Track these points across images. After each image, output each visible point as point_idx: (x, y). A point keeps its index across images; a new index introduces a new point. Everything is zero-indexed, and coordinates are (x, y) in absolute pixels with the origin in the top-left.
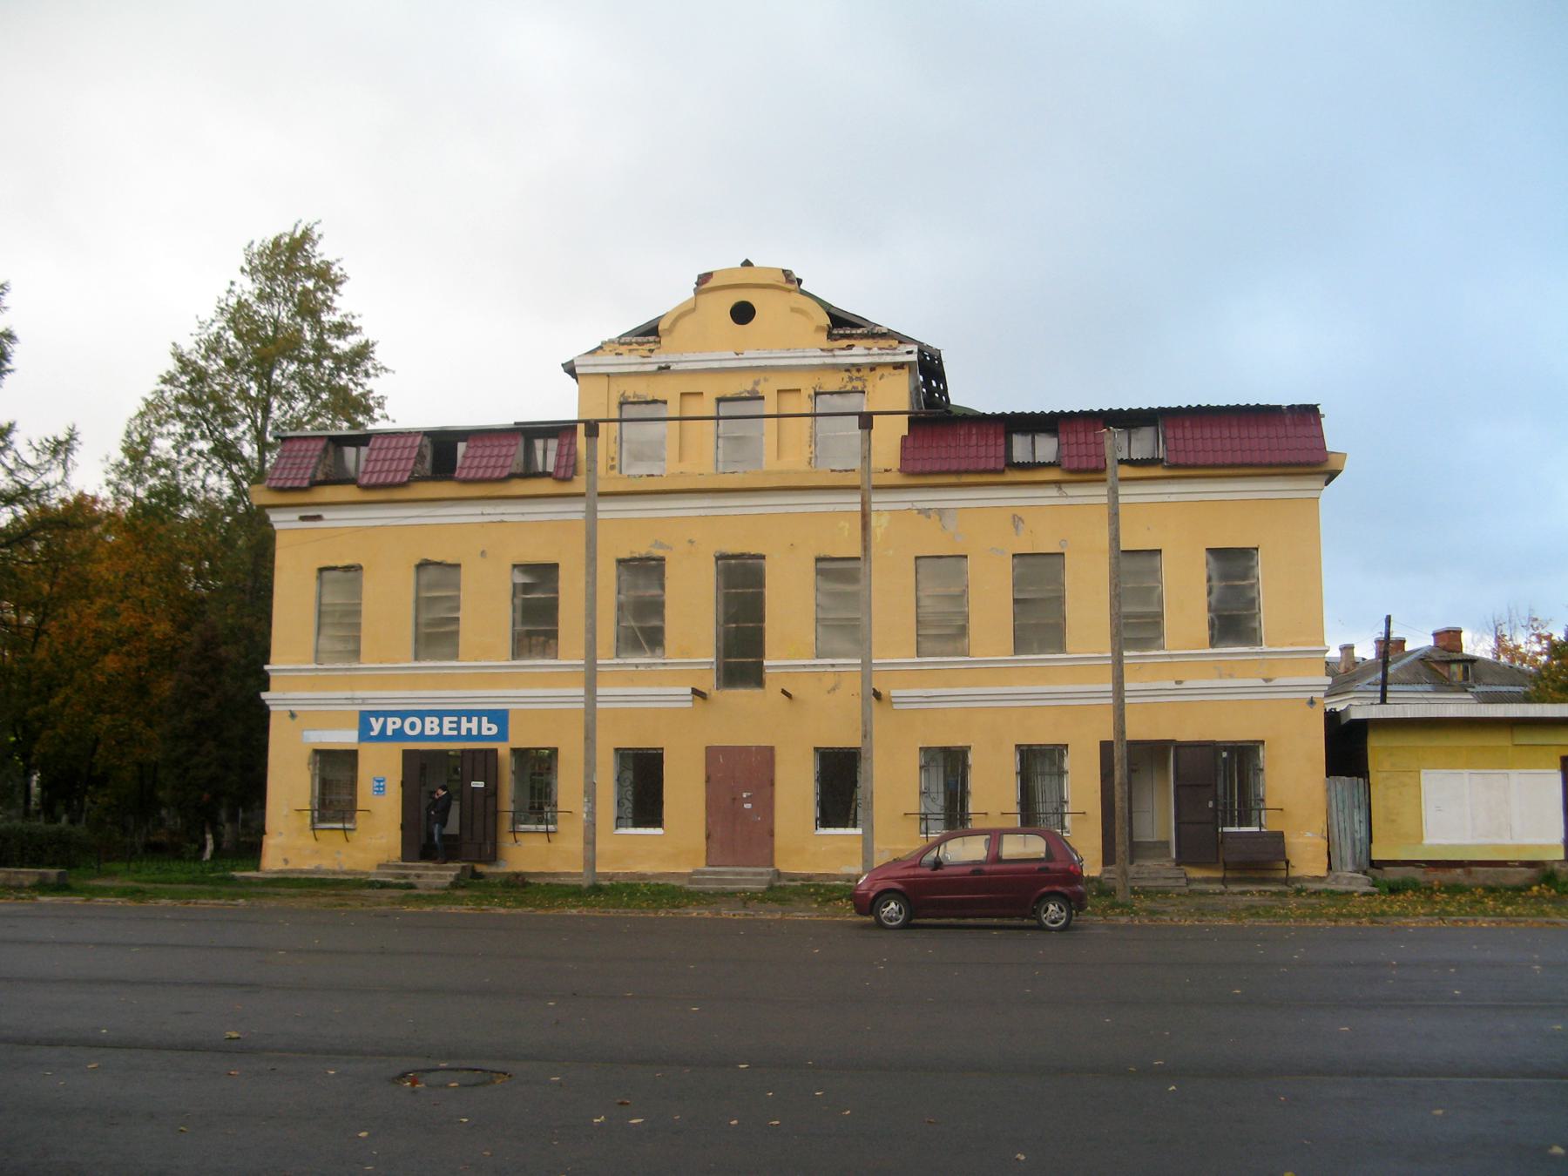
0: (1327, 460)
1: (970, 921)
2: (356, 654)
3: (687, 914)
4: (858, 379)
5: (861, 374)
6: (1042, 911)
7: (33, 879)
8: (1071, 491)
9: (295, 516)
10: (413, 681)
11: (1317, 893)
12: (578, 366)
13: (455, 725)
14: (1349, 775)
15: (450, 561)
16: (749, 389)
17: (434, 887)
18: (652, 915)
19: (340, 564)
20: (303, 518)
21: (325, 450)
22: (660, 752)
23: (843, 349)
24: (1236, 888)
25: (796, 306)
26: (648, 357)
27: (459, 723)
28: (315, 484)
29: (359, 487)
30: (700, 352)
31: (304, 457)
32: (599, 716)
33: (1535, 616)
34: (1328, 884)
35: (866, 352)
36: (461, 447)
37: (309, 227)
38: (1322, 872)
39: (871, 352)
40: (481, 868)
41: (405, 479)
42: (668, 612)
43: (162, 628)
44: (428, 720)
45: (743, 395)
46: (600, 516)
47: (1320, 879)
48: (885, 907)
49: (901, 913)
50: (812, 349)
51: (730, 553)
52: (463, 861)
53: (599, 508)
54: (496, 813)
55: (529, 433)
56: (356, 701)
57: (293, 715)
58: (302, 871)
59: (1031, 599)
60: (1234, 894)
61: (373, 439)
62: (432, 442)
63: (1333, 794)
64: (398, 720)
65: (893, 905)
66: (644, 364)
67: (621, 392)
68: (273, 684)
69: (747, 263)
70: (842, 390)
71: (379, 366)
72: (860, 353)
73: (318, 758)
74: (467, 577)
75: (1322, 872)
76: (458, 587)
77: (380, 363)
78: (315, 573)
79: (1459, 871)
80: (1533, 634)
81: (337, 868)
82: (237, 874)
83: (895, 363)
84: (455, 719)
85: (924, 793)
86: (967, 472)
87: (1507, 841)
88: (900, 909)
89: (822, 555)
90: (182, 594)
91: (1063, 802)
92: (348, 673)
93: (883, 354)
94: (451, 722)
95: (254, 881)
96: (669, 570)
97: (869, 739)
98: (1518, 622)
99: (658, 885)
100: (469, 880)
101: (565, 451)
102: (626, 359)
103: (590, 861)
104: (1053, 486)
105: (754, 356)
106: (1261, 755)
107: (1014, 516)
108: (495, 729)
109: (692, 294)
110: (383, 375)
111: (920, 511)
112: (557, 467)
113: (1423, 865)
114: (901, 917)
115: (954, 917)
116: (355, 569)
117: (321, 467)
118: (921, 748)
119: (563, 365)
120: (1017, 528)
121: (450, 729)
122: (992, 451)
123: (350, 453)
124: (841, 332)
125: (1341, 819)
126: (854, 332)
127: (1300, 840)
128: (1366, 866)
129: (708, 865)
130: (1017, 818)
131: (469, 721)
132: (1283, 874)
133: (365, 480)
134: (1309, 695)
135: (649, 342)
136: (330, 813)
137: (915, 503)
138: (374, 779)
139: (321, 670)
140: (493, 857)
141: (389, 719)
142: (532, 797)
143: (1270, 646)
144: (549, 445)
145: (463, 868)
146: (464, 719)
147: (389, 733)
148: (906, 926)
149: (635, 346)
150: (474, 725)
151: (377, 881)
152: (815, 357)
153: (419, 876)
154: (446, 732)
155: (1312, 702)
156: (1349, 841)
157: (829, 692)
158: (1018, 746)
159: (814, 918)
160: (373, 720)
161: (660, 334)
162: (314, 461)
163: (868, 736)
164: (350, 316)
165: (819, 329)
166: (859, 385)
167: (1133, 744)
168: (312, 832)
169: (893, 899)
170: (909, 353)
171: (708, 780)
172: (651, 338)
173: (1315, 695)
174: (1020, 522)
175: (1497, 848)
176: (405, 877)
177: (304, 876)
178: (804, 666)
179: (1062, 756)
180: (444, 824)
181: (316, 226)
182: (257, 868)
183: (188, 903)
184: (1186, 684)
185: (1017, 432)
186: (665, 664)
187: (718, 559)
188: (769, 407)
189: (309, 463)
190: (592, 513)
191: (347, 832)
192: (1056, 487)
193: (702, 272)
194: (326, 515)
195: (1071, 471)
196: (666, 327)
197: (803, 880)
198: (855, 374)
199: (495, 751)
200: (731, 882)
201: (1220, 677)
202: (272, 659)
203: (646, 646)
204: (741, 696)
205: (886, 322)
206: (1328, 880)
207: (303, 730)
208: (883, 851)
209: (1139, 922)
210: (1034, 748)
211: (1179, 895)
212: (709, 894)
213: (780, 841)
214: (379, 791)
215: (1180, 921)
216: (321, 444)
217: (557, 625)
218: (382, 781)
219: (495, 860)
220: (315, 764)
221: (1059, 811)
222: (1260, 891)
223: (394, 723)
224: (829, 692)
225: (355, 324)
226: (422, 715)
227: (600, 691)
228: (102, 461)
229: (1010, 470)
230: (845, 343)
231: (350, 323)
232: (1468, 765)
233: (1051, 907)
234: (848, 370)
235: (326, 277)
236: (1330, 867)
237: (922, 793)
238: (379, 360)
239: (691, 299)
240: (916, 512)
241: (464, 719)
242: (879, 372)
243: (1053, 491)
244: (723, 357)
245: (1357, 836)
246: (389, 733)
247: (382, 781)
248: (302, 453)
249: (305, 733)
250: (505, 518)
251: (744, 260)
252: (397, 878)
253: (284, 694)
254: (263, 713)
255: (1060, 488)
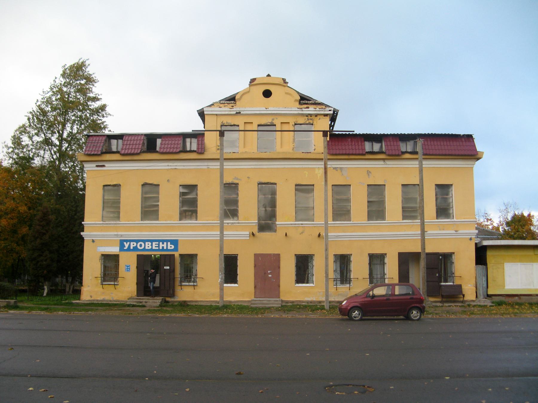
0: (478, 154)
1: (375, 317)
2: (118, 218)
3: (269, 316)
4: (311, 119)
5: (312, 118)
6: (411, 313)
7: (5, 304)
8: (388, 162)
9: (95, 165)
10: (141, 229)
11: (474, 306)
12: (205, 111)
13: (157, 245)
14: (481, 265)
15: (155, 183)
16: (270, 122)
17: (153, 306)
18: (256, 317)
19: (112, 184)
20: (97, 166)
21: (106, 140)
22: (236, 256)
23: (306, 108)
24: (447, 305)
25: (287, 92)
26: (232, 109)
27: (159, 244)
28: (103, 153)
29: (120, 154)
30: (252, 107)
31: (98, 143)
32: (224, 241)
33: (486, 213)
34: (477, 303)
35: (314, 110)
36: (159, 141)
37: (84, 61)
38: (474, 298)
39: (316, 110)
40: (168, 299)
41: (139, 152)
42: (240, 204)
43: (23, 209)
44: (147, 243)
45: (268, 124)
46: (225, 167)
47: (473, 301)
48: (354, 312)
49: (359, 315)
50: (295, 108)
51: (263, 182)
52: (162, 296)
53: (224, 164)
54: (174, 278)
55: (185, 136)
56: (119, 236)
57: (93, 241)
58: (97, 300)
59: (371, 201)
60: (446, 306)
61: (124, 137)
62: (146, 138)
63: (477, 271)
64: (135, 244)
65: (356, 312)
66: (231, 111)
67: (222, 121)
68: (85, 229)
69: (269, 75)
70: (305, 123)
71: (108, 113)
72: (311, 110)
73: (103, 258)
74: (162, 189)
75: (474, 298)
76: (158, 193)
77: (108, 112)
78: (102, 187)
79: (517, 298)
80: (485, 219)
81: (111, 299)
82: (74, 302)
83: (324, 114)
84: (158, 243)
85: (335, 271)
86: (353, 154)
87: (532, 287)
88: (359, 313)
89: (298, 184)
90: (30, 196)
91: (384, 274)
92: (115, 225)
93: (320, 111)
94: (155, 244)
95: (80, 304)
96: (240, 187)
97: (327, 251)
98: (481, 214)
99: (238, 305)
100: (165, 303)
101: (200, 142)
102: (223, 109)
103: (222, 297)
104: (382, 160)
105: (272, 110)
106: (453, 257)
107: (368, 171)
108: (173, 247)
109: (248, 86)
110: (109, 117)
111: (334, 168)
112: (198, 148)
113: (505, 296)
114: (360, 316)
115: (385, 316)
116: (118, 186)
117: (104, 147)
118: (334, 255)
119: (197, 111)
120: (369, 175)
121: (156, 247)
122: (350, 147)
123: (114, 142)
124: (304, 102)
125: (480, 280)
126: (309, 102)
127: (466, 287)
128: (486, 297)
129: (255, 297)
130: (368, 280)
131: (163, 244)
132: (462, 299)
133: (123, 152)
134: (470, 237)
135: (231, 103)
136: (107, 279)
137: (332, 165)
138: (126, 266)
139: (104, 224)
140: (173, 295)
141: (153, 243)
142: (185, 273)
143: (457, 219)
144: (192, 140)
145: (162, 299)
146: (161, 243)
147: (132, 248)
148: (361, 320)
149: (226, 105)
150: (165, 245)
151: (130, 304)
152: (295, 111)
153: (146, 302)
154: (154, 248)
155: (471, 239)
156: (482, 287)
157: (300, 234)
158: (295, 255)
159: (318, 317)
160: (125, 243)
161: (236, 100)
162: (102, 144)
163: (327, 250)
164: (98, 95)
165: (296, 100)
166: (311, 122)
167: (428, 254)
168: (101, 285)
169: (356, 310)
170: (330, 110)
171: (255, 266)
172: (233, 102)
173: (472, 237)
174: (370, 174)
175: (529, 290)
176: (141, 302)
177: (100, 302)
178: (291, 224)
179: (384, 258)
180: (154, 283)
181: (87, 61)
182: (79, 299)
183: (70, 313)
184: (460, 232)
185: (367, 141)
186: (238, 223)
187: (258, 184)
188: (278, 128)
189: (100, 145)
190: (222, 166)
191: (115, 285)
192: (383, 161)
193: (252, 78)
194: (106, 165)
195: (389, 155)
196: (239, 98)
197: (291, 303)
198: (310, 117)
199: (174, 255)
200: (267, 304)
201: (440, 230)
202: (85, 220)
203: (230, 216)
204: (266, 235)
205: (320, 100)
206: (476, 301)
207: (97, 247)
208: (320, 292)
209: (436, 317)
210: (374, 255)
211: (429, 307)
212: (260, 308)
213: (282, 288)
214: (128, 270)
215: (449, 316)
216: (104, 138)
217: (197, 207)
218: (129, 266)
219: (174, 296)
220: (102, 259)
221: (383, 278)
222: (455, 306)
223: (133, 244)
224: (300, 234)
225: (99, 97)
226: (144, 241)
227: (225, 233)
228: (2, 143)
229: (367, 154)
230: (306, 106)
231: (98, 97)
232: (521, 261)
233: (414, 312)
234: (307, 116)
235: (90, 80)
236: (477, 297)
237: (334, 271)
238: (108, 111)
239: (248, 88)
240: (332, 168)
241: (161, 243)
242: (318, 117)
243: (382, 162)
244: (261, 110)
245: (484, 286)
246: (132, 248)
247: (129, 266)
248: (97, 141)
249: (98, 248)
250: (177, 167)
251: (268, 74)
252: (138, 303)
253: (90, 233)
254: (82, 239)
255: (384, 161)
